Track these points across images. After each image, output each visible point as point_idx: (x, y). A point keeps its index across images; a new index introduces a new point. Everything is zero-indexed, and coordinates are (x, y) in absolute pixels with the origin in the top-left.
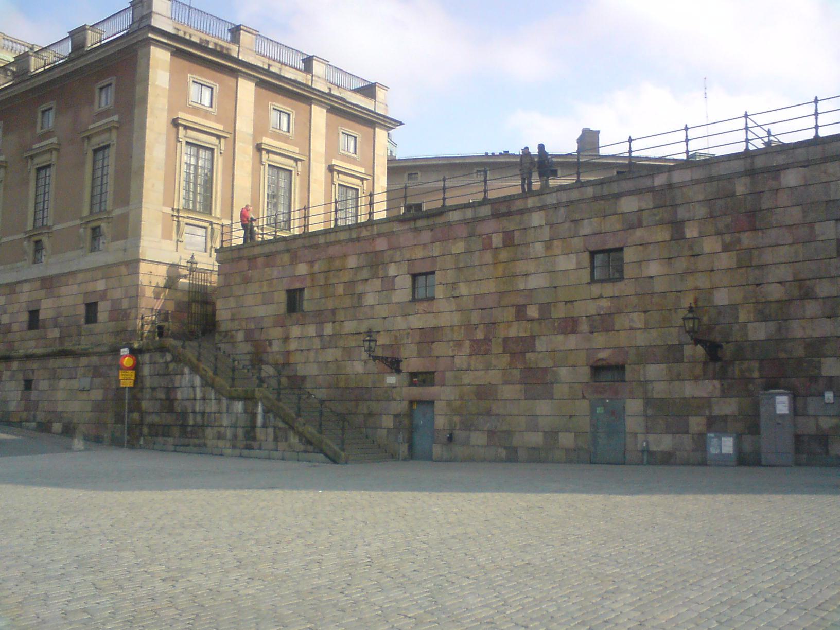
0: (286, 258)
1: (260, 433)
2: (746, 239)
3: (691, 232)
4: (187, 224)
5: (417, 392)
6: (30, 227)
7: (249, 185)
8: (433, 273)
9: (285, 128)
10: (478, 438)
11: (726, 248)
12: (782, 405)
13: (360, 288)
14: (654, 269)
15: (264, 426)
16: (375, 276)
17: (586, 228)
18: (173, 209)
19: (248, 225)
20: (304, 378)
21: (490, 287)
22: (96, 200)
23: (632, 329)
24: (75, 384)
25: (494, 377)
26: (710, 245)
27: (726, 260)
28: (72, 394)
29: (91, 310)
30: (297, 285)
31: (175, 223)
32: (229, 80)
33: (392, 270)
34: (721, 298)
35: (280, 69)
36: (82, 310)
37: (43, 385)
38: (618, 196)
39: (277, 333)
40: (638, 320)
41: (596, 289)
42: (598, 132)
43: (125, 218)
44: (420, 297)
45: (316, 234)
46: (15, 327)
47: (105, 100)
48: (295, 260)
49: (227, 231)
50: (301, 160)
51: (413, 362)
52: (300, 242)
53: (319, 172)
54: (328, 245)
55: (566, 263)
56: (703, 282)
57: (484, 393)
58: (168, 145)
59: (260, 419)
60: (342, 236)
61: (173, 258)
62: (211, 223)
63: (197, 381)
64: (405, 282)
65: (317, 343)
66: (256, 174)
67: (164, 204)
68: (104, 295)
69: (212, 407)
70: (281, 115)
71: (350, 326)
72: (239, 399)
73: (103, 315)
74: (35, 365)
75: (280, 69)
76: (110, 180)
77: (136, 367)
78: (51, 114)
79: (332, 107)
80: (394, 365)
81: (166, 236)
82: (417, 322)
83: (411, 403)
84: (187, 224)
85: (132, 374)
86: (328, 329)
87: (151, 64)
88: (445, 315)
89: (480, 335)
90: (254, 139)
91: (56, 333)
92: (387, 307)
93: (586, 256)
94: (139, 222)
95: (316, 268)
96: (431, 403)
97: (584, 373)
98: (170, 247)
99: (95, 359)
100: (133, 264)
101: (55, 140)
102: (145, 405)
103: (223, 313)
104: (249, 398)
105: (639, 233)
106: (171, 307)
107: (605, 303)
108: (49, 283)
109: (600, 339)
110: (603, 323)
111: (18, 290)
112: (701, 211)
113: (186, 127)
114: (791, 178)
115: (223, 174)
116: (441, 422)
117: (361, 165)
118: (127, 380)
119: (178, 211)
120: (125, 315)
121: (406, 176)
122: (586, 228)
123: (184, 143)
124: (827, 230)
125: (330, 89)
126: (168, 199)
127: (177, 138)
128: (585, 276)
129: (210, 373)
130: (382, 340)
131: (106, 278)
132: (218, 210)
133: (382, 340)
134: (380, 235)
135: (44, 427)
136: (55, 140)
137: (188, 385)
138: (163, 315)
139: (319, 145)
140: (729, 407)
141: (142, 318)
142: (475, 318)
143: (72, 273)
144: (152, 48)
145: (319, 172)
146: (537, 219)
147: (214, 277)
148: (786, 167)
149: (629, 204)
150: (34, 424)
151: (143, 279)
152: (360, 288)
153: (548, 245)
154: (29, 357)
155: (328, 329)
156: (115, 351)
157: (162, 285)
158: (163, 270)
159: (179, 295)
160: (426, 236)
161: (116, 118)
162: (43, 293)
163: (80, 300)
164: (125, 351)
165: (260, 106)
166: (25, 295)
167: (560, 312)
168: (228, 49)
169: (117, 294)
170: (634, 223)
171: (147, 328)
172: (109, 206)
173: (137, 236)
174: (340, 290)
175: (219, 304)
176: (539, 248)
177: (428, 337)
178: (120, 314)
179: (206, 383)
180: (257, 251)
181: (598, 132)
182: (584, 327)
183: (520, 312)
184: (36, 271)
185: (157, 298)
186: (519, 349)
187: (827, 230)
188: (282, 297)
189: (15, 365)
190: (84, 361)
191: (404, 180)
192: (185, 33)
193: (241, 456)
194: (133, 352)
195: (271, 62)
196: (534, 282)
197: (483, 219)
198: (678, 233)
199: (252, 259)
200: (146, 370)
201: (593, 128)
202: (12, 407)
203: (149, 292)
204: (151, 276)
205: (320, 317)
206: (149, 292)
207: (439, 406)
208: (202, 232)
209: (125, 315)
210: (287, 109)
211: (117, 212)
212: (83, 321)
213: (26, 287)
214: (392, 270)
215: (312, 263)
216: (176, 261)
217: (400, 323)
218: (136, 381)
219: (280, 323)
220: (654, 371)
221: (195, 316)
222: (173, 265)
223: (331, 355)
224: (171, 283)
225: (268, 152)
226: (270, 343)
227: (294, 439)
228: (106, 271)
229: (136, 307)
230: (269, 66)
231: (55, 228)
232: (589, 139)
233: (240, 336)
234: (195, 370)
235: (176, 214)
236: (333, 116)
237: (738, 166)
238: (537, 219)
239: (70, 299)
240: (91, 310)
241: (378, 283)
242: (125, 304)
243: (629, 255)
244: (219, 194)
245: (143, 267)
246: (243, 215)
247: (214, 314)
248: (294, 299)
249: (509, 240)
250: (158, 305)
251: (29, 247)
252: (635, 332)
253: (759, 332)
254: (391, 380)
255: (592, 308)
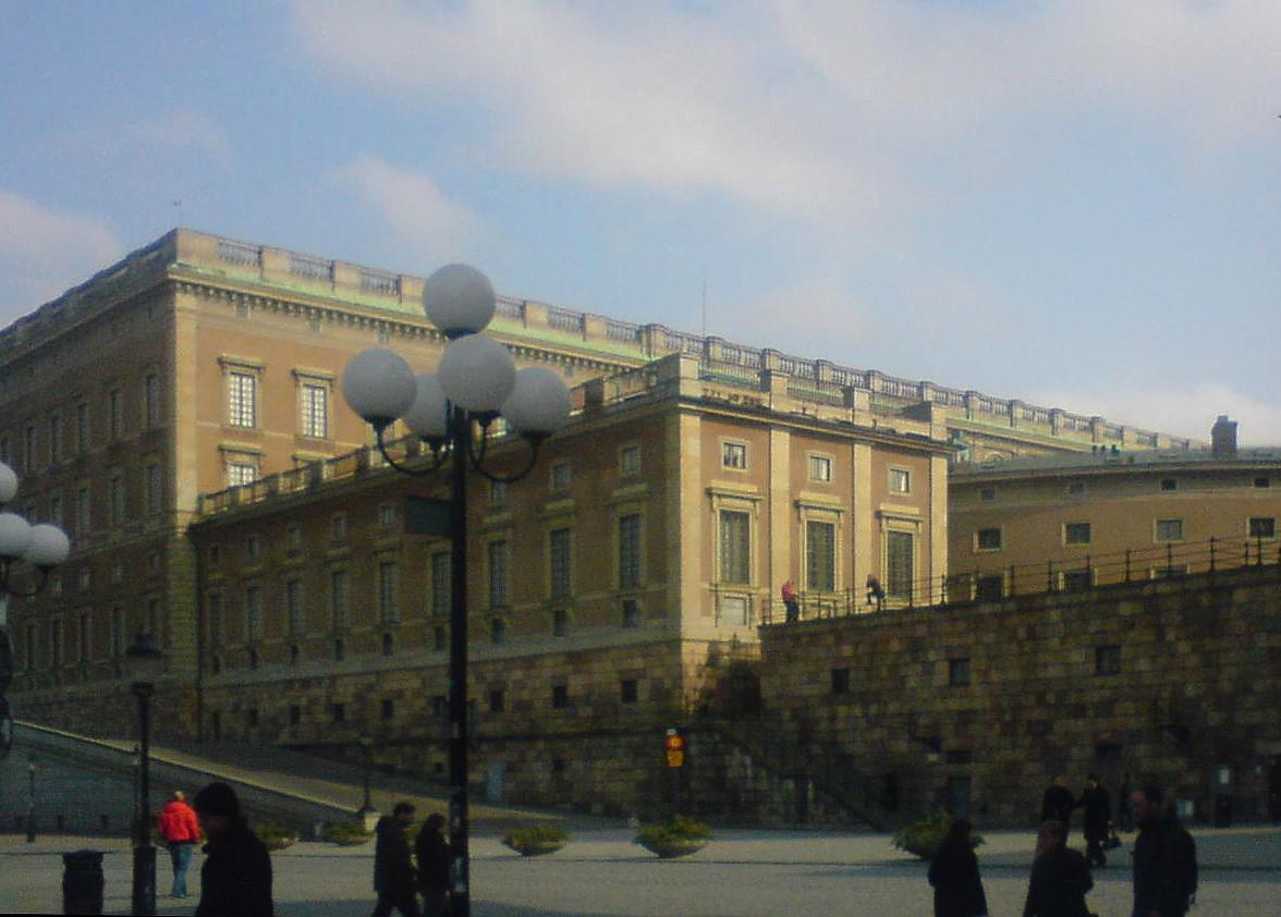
0: (830, 639)
1: (811, 808)
2: (1209, 644)
3: (1170, 636)
4: (726, 598)
5: (953, 769)
6: (548, 594)
7: (787, 547)
8: (968, 660)
9: (824, 477)
10: (1007, 809)
11: (1194, 649)
12: (1225, 777)
13: (903, 672)
14: (1143, 665)
15: (817, 800)
16: (915, 660)
17: (1094, 626)
18: (711, 584)
19: (791, 605)
20: (851, 757)
21: (1014, 675)
22: (629, 578)
23: (1126, 715)
24: (615, 764)
25: (1020, 755)
26: (1183, 647)
27: (1193, 660)
28: (610, 773)
29: (629, 689)
30: (842, 666)
31: (714, 599)
32: (761, 435)
33: (932, 656)
34: (1190, 691)
35: (816, 411)
36: (617, 688)
37: (577, 765)
38: (1117, 601)
39: (823, 712)
40: (1130, 707)
41: (1098, 681)
42: (1235, 424)
43: (661, 596)
44: (957, 679)
45: (860, 617)
46: (539, 704)
47: (631, 462)
48: (839, 641)
49: (767, 602)
50: (843, 511)
51: (951, 743)
52: (842, 625)
53: (864, 521)
54: (875, 628)
55: (1077, 657)
56: (1175, 677)
57: (1013, 768)
58: (702, 517)
59: (811, 795)
60: (885, 620)
61: (714, 635)
62: (750, 595)
63: (748, 761)
64: (943, 668)
65: (863, 723)
66: (794, 532)
67: (702, 580)
68: (642, 674)
69: (764, 785)
70: (821, 463)
71: (893, 707)
72: (789, 776)
73: (643, 691)
74: (566, 745)
75: (816, 411)
76: (643, 553)
77: (684, 748)
78: (567, 471)
79: (877, 442)
80: (934, 744)
81: (706, 613)
82: (953, 704)
83: (951, 779)
84: (726, 598)
85: (680, 755)
86: (873, 709)
87: (682, 432)
88: (981, 701)
89: (1008, 717)
90: (791, 494)
91: (589, 711)
92: (927, 685)
93: (1092, 652)
94: (678, 602)
95: (861, 649)
96: (968, 779)
97: (1090, 751)
98: (713, 622)
99: (636, 739)
100: (674, 644)
101: (570, 503)
102: (693, 784)
103: (768, 688)
104: (800, 777)
105: (1132, 634)
106: (713, 684)
107: (1107, 693)
108: (576, 659)
109: (1102, 724)
110: (1106, 708)
111: (538, 663)
112: (1178, 619)
113: (719, 496)
114: (1240, 596)
115: (737, 436)
116: (975, 795)
117: (913, 504)
118: (675, 760)
119: (716, 585)
120: (668, 694)
121: (979, 495)
122: (1094, 626)
123: (718, 513)
124: (1262, 641)
125: (875, 421)
126: (706, 573)
127: (712, 507)
128: (1092, 668)
129: (761, 753)
130: (923, 721)
131: (645, 656)
132: (756, 580)
133: (923, 721)
134: (919, 622)
135: (582, 809)
136: (570, 503)
137: (739, 764)
138: (707, 694)
139: (863, 490)
140: (1191, 779)
141: (686, 698)
142: (1005, 704)
143: (607, 649)
144: (682, 417)
145: (864, 521)
146: (1054, 616)
147: (759, 652)
148: (1235, 587)
149: (1126, 609)
150: (569, 806)
151: (686, 658)
152: (903, 672)
153: (1063, 640)
154: (562, 737)
155: (873, 709)
156: (660, 731)
157: (703, 663)
158: (705, 646)
159: (720, 673)
160: (961, 626)
161: (641, 487)
162: (570, 668)
163: (615, 676)
164: (671, 732)
165: (796, 455)
166: (547, 670)
167: (1073, 699)
168: (759, 400)
169: (658, 672)
170: (1129, 624)
171: (691, 708)
172: (642, 580)
173: (677, 616)
174: (884, 673)
175: (764, 683)
176: (1055, 642)
177: (965, 718)
178: (663, 694)
179: (758, 763)
180: (800, 630)
181: (1235, 424)
182: (1090, 713)
183: (1041, 699)
184: (560, 645)
185: (699, 676)
186: (1040, 730)
187: (1262, 641)
188: (826, 677)
189: (541, 745)
190: (624, 741)
191: (976, 502)
192: (713, 392)
193: (1032, 472)
194: (681, 733)
195: (806, 404)
196: (1052, 672)
197: (1009, 614)
198: (1160, 636)
199: (797, 638)
200: (693, 750)
201: (1231, 419)
202: (542, 787)
203: (692, 672)
204: (693, 654)
205: (865, 699)
206: (692, 672)
207: (975, 782)
208: (739, 604)
209: (668, 694)
210: (826, 454)
211: (653, 588)
212: (619, 697)
213: (548, 662)
214: (932, 656)
215: (856, 644)
216: (717, 638)
217: (939, 706)
218: (684, 762)
219: (826, 700)
220: (1142, 750)
221: (738, 688)
222: (713, 644)
223: (877, 734)
224: (713, 659)
225: (806, 508)
226: (817, 721)
227: (843, 813)
228: (645, 648)
229: (681, 688)
230: (804, 409)
231: (579, 599)
232: (1225, 431)
233: (787, 714)
234: (745, 750)
235: (713, 588)
236: (882, 454)
237: (1203, 583)
238: (1054, 616)
239: (604, 674)
240: (629, 689)
241: (919, 668)
242: (668, 683)
243: (1126, 652)
244: (756, 550)
245: (686, 647)
246: (785, 593)
247: (757, 689)
248: (840, 681)
249: (1032, 634)
250: (701, 684)
251: (549, 618)
252: (1129, 717)
253: (1215, 718)
254: (933, 757)
255: (1096, 696)
